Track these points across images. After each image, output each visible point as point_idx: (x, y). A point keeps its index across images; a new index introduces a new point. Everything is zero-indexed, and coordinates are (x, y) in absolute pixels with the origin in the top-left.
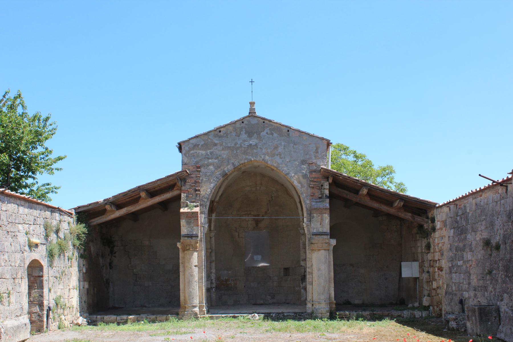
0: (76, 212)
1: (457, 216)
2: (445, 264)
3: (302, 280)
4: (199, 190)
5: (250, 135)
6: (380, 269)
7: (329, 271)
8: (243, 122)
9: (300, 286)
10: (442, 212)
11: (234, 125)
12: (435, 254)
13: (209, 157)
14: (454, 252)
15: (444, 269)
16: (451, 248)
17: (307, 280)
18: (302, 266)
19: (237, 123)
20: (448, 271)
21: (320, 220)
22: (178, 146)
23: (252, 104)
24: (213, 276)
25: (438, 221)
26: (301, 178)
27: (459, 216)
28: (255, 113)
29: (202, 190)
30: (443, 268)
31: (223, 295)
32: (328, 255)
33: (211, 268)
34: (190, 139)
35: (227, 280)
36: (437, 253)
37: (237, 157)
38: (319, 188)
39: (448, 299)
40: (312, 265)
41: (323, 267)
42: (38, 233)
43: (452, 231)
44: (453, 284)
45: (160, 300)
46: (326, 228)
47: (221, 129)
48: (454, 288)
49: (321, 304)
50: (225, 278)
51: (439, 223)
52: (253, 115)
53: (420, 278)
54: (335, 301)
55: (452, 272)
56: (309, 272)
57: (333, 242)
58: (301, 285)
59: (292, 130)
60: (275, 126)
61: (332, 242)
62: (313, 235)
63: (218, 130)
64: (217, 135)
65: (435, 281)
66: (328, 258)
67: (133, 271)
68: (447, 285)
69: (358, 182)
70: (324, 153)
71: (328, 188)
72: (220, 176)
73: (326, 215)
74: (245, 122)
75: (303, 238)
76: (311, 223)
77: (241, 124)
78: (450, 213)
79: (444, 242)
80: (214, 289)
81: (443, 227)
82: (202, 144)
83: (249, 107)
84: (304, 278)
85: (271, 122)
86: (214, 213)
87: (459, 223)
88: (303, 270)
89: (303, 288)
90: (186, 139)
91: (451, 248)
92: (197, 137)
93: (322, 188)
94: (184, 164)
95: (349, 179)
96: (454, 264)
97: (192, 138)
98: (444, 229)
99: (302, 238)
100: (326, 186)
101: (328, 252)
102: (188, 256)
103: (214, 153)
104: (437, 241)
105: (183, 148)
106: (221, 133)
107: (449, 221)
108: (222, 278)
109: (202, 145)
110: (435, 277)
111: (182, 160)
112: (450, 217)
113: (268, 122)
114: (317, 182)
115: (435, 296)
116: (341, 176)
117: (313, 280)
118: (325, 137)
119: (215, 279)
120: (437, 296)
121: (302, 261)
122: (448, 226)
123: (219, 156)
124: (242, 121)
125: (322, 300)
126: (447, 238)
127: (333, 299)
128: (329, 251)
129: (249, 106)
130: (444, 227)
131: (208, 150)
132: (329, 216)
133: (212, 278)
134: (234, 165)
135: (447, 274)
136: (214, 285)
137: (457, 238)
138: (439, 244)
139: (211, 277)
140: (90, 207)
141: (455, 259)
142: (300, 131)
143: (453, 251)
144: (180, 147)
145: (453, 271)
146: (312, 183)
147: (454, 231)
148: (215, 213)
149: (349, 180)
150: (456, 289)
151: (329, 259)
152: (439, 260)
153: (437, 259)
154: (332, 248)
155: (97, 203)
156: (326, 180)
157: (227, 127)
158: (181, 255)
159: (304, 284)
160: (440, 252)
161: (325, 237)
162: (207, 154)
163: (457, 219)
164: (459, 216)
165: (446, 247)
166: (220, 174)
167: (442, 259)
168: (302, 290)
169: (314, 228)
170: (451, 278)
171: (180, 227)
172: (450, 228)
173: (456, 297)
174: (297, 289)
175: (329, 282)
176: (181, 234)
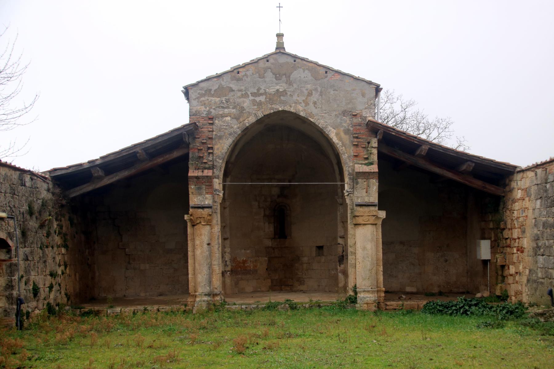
0: (51, 176)
1: (546, 183)
2: (526, 243)
3: (339, 261)
4: (212, 148)
5: (278, 77)
6: (438, 248)
7: (377, 251)
8: (268, 61)
9: (337, 269)
10: (524, 178)
11: (256, 64)
12: (513, 230)
13: (224, 106)
14: (541, 229)
15: (526, 250)
16: (536, 223)
17: (349, 262)
18: (339, 244)
19: (260, 61)
20: (531, 253)
21: (365, 186)
22: (185, 91)
23: (280, 36)
24: (227, 257)
25: (518, 189)
26: (342, 134)
27: (549, 182)
28: (284, 48)
29: (216, 147)
30: (524, 248)
31: (240, 280)
32: (375, 230)
33: (225, 246)
34: (199, 83)
35: (244, 262)
36: (516, 230)
37: (260, 106)
38: (364, 146)
39: (532, 289)
40: (355, 243)
41: (370, 246)
42: (2, 204)
43: (539, 202)
44: (539, 269)
45: (159, 287)
46: (374, 198)
47: (240, 70)
48: (540, 275)
49: (355, 286)
50: (242, 259)
51: (519, 191)
52: (282, 51)
53: (491, 261)
54: (384, 288)
55: (538, 254)
56: (352, 252)
57: (383, 214)
58: (339, 268)
59: (331, 71)
60: (309, 66)
61: (380, 215)
62: (357, 205)
63: (236, 71)
64: (234, 77)
65: (513, 265)
66: (375, 235)
67: (125, 250)
68: (530, 271)
69: (415, 139)
70: (372, 102)
71: (377, 146)
72: (238, 130)
73: (374, 180)
74: (271, 60)
75: (341, 208)
76: (355, 190)
77: (265, 64)
78: (537, 179)
79: (527, 216)
80: (228, 273)
81: (526, 196)
82: (215, 89)
83: (276, 41)
84: (342, 259)
85: (304, 60)
86: (228, 177)
87: (550, 192)
88: (340, 250)
89: (341, 272)
90: (194, 81)
91: (536, 223)
92: (208, 79)
93: (369, 146)
94: (192, 114)
95: (404, 135)
96: (540, 244)
97: (202, 81)
98: (527, 199)
99: (340, 209)
100: (374, 143)
101: (376, 228)
102: (198, 232)
103: (231, 100)
104: (517, 214)
105: (190, 93)
106: (240, 75)
107: (534, 189)
108: (239, 259)
109: (214, 90)
110: (514, 260)
111: (190, 109)
112: (536, 184)
113: (300, 61)
114: (362, 139)
115: (513, 283)
116: (394, 131)
117: (357, 262)
118: (374, 81)
119: (230, 261)
120: (515, 284)
121: (340, 237)
122: (532, 196)
123: (238, 104)
124: (266, 58)
125: (368, 287)
126: (531, 211)
127: (382, 286)
128: (377, 225)
129: (275, 39)
130: (527, 196)
131: (224, 97)
132: (377, 182)
133: (226, 259)
134: (257, 116)
135: (530, 256)
136: (229, 268)
137: (545, 212)
138: (518, 218)
139: (225, 258)
140: (69, 171)
141: (543, 238)
142: (341, 73)
143: (540, 227)
144: (187, 91)
145: (539, 253)
146: (355, 140)
147: (541, 202)
148: (230, 177)
149: (404, 136)
150: (542, 276)
151: (376, 236)
152: (519, 238)
153: (516, 237)
154: (380, 223)
155: (81, 165)
156: (375, 136)
157: (247, 67)
158: (189, 230)
159: (342, 266)
160: (520, 228)
161: (372, 208)
162: (222, 102)
163: (546, 187)
164: (549, 182)
165: (530, 221)
166: (239, 128)
167: (523, 237)
168: (340, 274)
169: (358, 197)
170: (536, 262)
171: (189, 194)
172: (535, 197)
173: (543, 285)
174: (333, 272)
175: (378, 265)
176: (190, 204)
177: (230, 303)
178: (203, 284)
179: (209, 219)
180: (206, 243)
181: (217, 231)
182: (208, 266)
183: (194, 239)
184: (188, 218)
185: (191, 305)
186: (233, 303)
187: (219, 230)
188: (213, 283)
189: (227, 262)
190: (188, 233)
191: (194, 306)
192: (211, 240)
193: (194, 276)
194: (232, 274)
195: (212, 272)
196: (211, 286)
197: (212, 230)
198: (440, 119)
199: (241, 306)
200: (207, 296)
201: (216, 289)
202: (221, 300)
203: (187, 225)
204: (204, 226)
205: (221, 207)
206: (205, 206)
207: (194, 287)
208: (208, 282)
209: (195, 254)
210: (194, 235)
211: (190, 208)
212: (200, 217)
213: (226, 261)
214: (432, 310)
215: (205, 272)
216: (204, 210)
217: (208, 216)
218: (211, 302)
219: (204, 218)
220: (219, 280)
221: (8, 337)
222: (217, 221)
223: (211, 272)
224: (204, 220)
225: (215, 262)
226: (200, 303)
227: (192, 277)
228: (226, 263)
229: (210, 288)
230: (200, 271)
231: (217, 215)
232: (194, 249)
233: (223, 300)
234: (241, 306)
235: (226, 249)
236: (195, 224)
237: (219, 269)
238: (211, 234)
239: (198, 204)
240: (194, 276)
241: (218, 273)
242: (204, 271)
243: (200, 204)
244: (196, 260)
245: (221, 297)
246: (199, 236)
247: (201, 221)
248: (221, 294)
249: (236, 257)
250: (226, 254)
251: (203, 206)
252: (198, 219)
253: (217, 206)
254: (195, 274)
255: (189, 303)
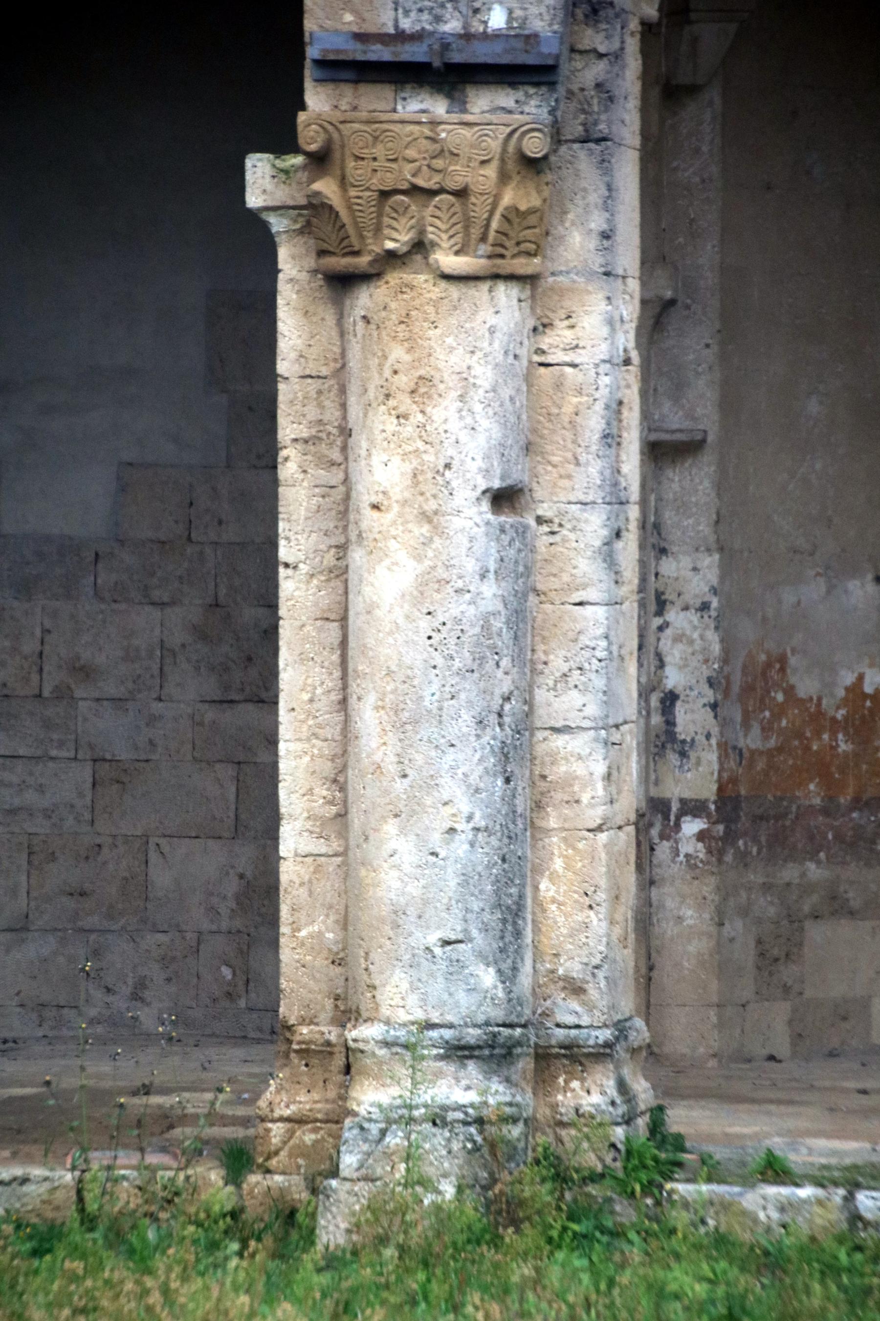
50: (849, 679)
80: (691, 827)
102: (398, 353)
119: (710, 695)
133: (673, 678)
176: (309, 25)
177: (719, 1153)
178: (433, 938)
179: (513, 216)
180: (483, 485)
181: (603, 350)
182: (493, 735)
183: (346, 432)
184: (282, 195)
185: (301, 1151)
186: (757, 1159)
187: (627, 339)
188: (537, 930)
189: (680, 711)
190: (282, 367)
191: (334, 1172)
192: (528, 448)
193: (336, 845)
194: (729, 837)
195: (538, 806)
196: (519, 951)
197: (545, 342)
198: (335, 562)
199: (850, 1198)
200: (472, 1067)
201: (576, 989)
202: (628, 1120)
203: (274, 271)
204: (454, 291)
205: (646, 77)
206: (482, 54)
207: (338, 961)
208: (493, 918)
209: (357, 605)
210: (343, 390)
211: (309, 73)
212: (414, 190)
213: (670, 699)
214: (602, 1233)
215: (464, 806)
216: (459, 103)
217: (504, 177)
218: (516, 1131)
219: (462, 193)
220: (601, 896)
221: (714, 674)
222: (606, 236)
223: (521, 804)
224: (467, 224)
225: (574, 698)
226: (395, 1140)
227: (321, 847)
228: (670, 723)
229: (508, 977)
230: (400, 786)
231: (604, 164)
232: (342, 549)
233: (642, 1122)
234: (850, 1198)
235: (668, 567)
236: (363, 261)
237: (608, 777)
238: (529, 378)
239: (401, 37)
240: (336, 845)
241: (595, 815)
242: (451, 788)
243: (417, 37)
244: (358, 664)
245: (622, 1087)
246: (405, 403)
247: (431, 235)
248: (620, 1050)
249: (783, 660)
250: (672, 615)
251: (457, 57)
252: (400, 211)
253: (616, 57)
254: (342, 815)
255: (277, 1130)
